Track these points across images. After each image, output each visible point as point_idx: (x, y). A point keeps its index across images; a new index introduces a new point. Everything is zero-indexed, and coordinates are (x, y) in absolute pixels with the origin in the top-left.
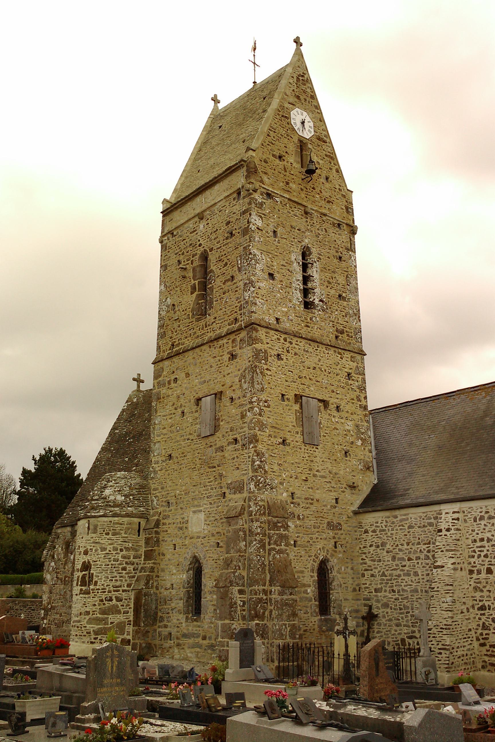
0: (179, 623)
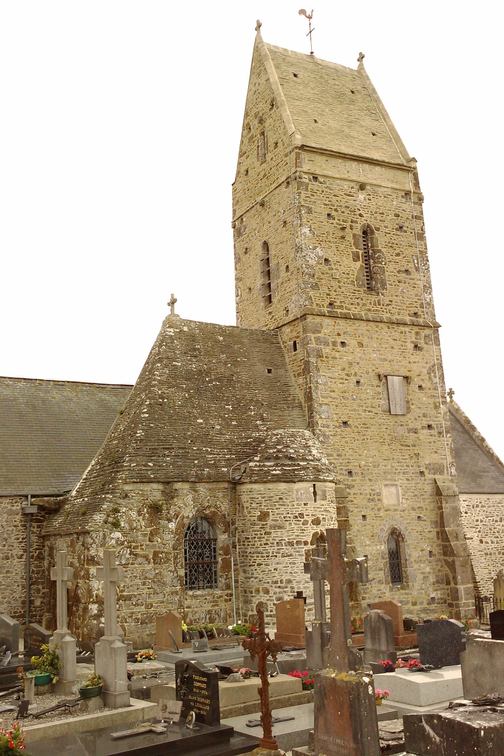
0: (382, 594)
